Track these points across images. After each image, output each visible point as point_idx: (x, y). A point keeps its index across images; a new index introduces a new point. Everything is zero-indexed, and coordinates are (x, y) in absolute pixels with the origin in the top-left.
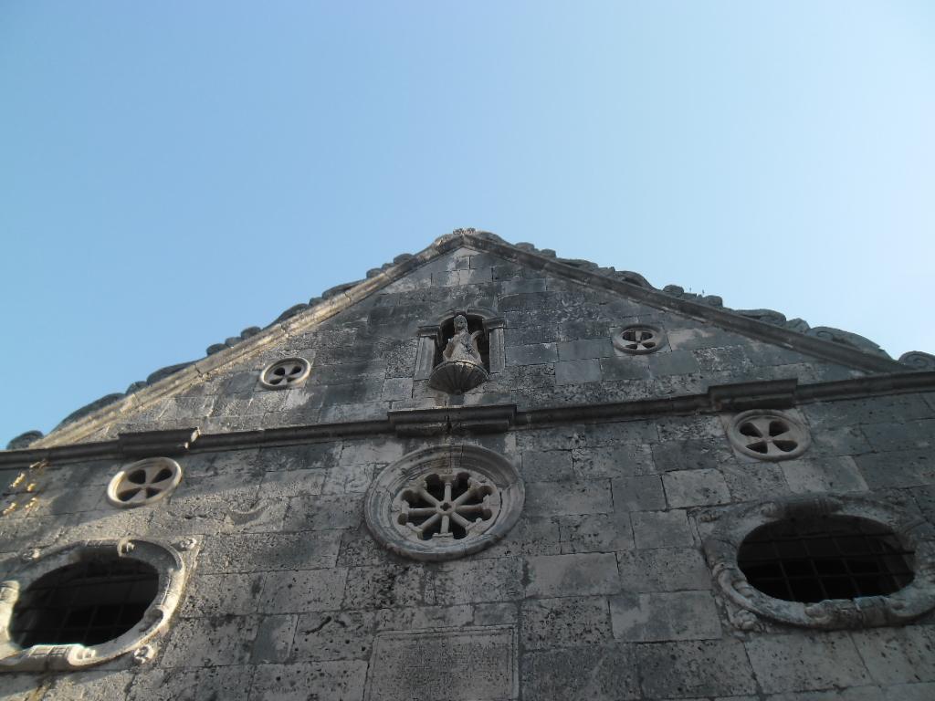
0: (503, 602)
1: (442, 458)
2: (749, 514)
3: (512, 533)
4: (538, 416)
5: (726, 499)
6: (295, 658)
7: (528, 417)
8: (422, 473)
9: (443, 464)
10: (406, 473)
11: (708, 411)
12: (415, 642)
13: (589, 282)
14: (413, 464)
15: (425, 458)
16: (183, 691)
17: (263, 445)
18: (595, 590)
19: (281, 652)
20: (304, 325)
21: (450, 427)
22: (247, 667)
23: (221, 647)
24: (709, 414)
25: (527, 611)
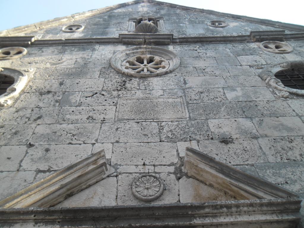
0: (176, 89)
1: (143, 51)
2: (275, 67)
3: (177, 70)
4: (181, 40)
5: (264, 63)
6: (81, 105)
7: (178, 41)
8: (134, 56)
9: (143, 53)
10: (127, 55)
11: (250, 41)
12: (137, 101)
13: (195, 11)
14: (131, 52)
15: (135, 51)
16: (25, 115)
17: (64, 45)
18: (217, 86)
19: (74, 103)
20: (81, 17)
21: (145, 42)
22: (57, 108)
23: (44, 101)
24: (251, 42)
25: (188, 92)
